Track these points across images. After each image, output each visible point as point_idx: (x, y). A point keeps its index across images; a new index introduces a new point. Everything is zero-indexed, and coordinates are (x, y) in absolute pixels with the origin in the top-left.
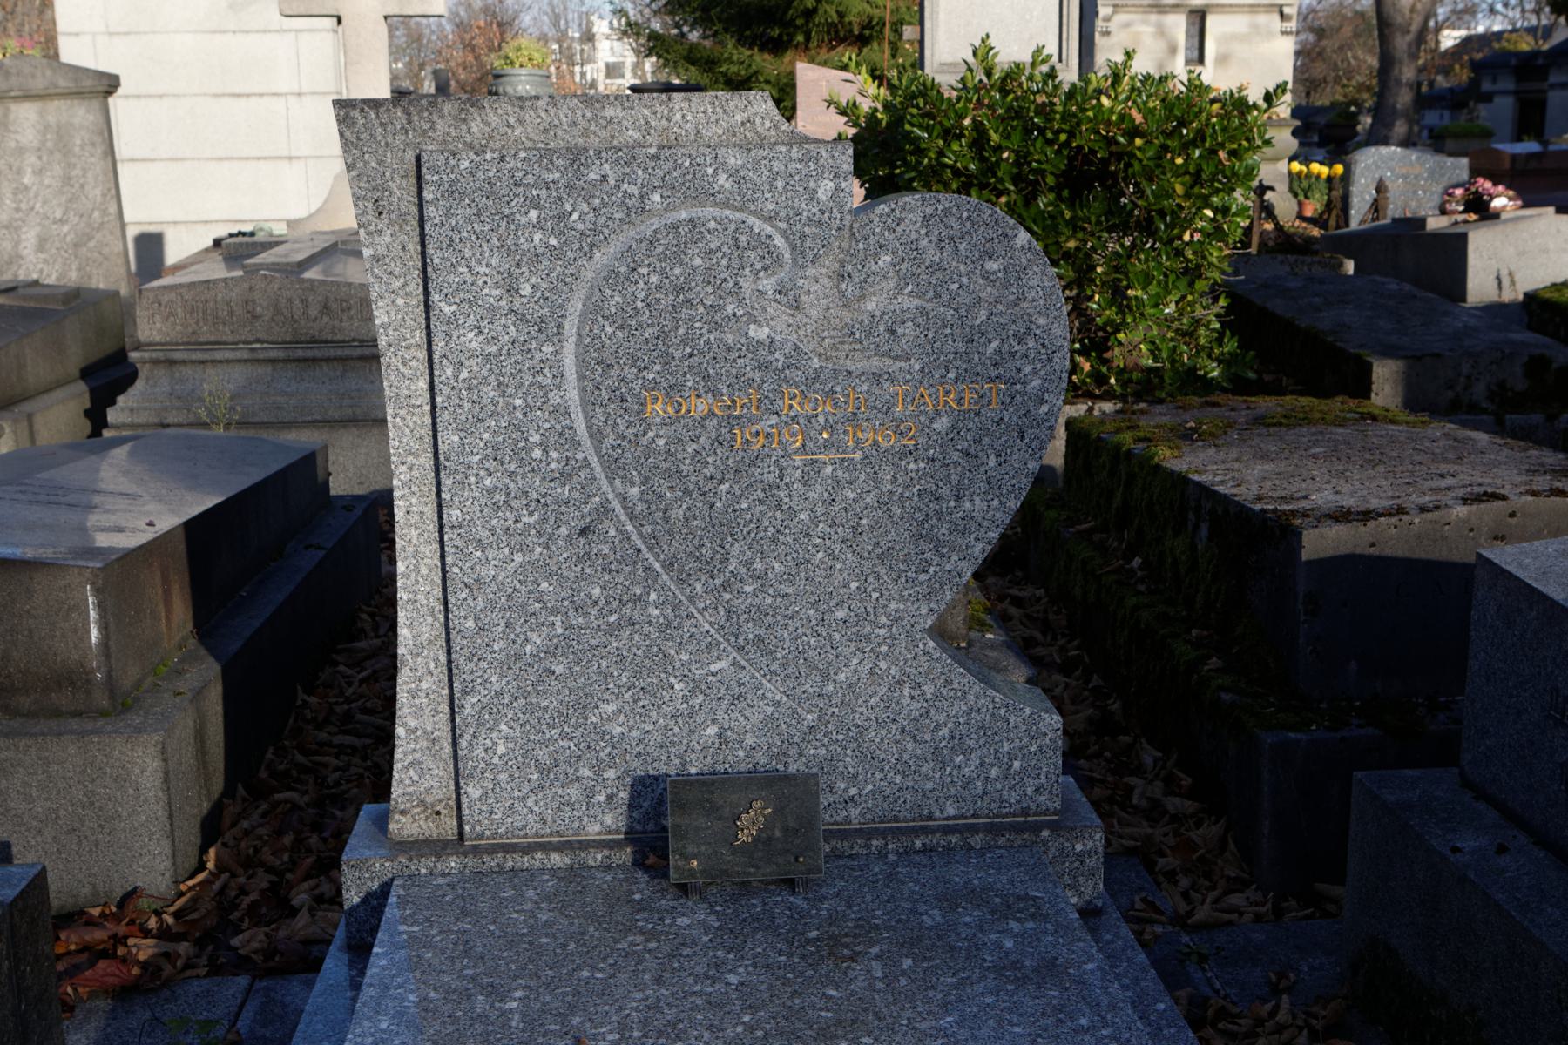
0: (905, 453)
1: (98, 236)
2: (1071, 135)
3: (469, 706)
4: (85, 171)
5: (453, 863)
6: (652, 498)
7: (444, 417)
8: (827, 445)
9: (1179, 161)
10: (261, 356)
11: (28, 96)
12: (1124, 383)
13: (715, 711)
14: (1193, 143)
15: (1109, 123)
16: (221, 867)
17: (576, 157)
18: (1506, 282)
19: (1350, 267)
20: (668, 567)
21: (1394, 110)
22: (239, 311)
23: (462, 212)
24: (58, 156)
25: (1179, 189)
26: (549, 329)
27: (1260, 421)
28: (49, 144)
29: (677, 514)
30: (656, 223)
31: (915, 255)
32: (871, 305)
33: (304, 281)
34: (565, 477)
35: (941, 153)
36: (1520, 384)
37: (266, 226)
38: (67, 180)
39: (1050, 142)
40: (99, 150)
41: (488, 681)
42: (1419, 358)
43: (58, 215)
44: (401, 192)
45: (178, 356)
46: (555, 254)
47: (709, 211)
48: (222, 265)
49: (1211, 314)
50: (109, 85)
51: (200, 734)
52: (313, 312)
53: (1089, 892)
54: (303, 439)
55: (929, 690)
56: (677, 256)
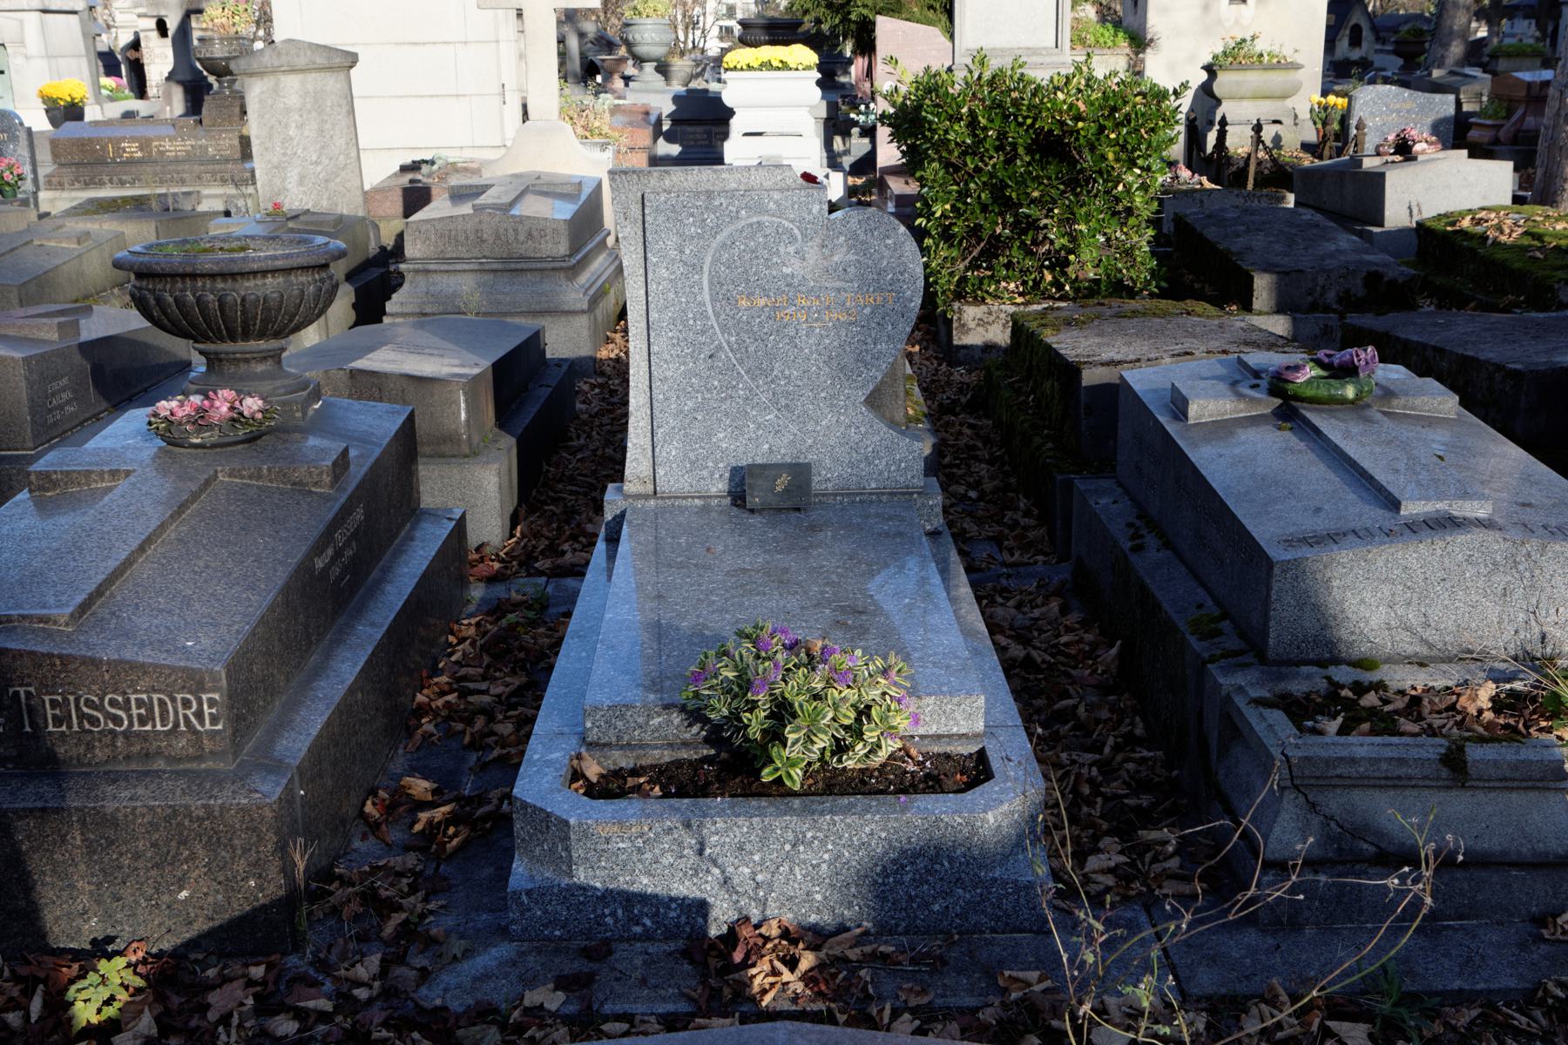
0: (850, 324)
1: (343, 174)
2: (1035, 120)
3: (660, 433)
4: (334, 125)
5: (652, 502)
6: (740, 342)
7: (652, 306)
8: (817, 320)
9: (1113, 136)
10: (487, 267)
11: (293, 70)
12: (1077, 290)
13: (765, 440)
14: (1121, 124)
15: (1061, 112)
16: (523, 535)
17: (709, 194)
18: (1415, 211)
19: (1290, 200)
20: (747, 372)
21: (1451, 32)
22: (472, 237)
23: (661, 219)
24: (314, 114)
25: (1111, 156)
26: (696, 268)
27: (1120, 315)
28: (308, 106)
29: (752, 349)
30: (743, 223)
31: (855, 237)
32: (836, 258)
33: (513, 216)
34: (703, 332)
35: (946, 132)
36: (1361, 292)
37: (444, 153)
38: (321, 131)
39: (1020, 125)
40: (344, 110)
41: (667, 423)
42: (1287, 273)
43: (314, 158)
44: (635, 210)
45: (431, 267)
46: (700, 236)
47: (765, 218)
48: (449, 203)
49: (1143, 240)
50: (352, 60)
51: (510, 470)
52: (522, 238)
53: (936, 524)
54: (530, 323)
55: (863, 430)
56: (752, 238)
